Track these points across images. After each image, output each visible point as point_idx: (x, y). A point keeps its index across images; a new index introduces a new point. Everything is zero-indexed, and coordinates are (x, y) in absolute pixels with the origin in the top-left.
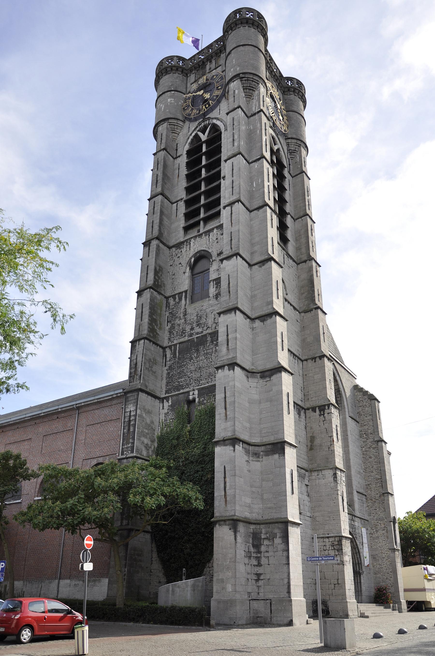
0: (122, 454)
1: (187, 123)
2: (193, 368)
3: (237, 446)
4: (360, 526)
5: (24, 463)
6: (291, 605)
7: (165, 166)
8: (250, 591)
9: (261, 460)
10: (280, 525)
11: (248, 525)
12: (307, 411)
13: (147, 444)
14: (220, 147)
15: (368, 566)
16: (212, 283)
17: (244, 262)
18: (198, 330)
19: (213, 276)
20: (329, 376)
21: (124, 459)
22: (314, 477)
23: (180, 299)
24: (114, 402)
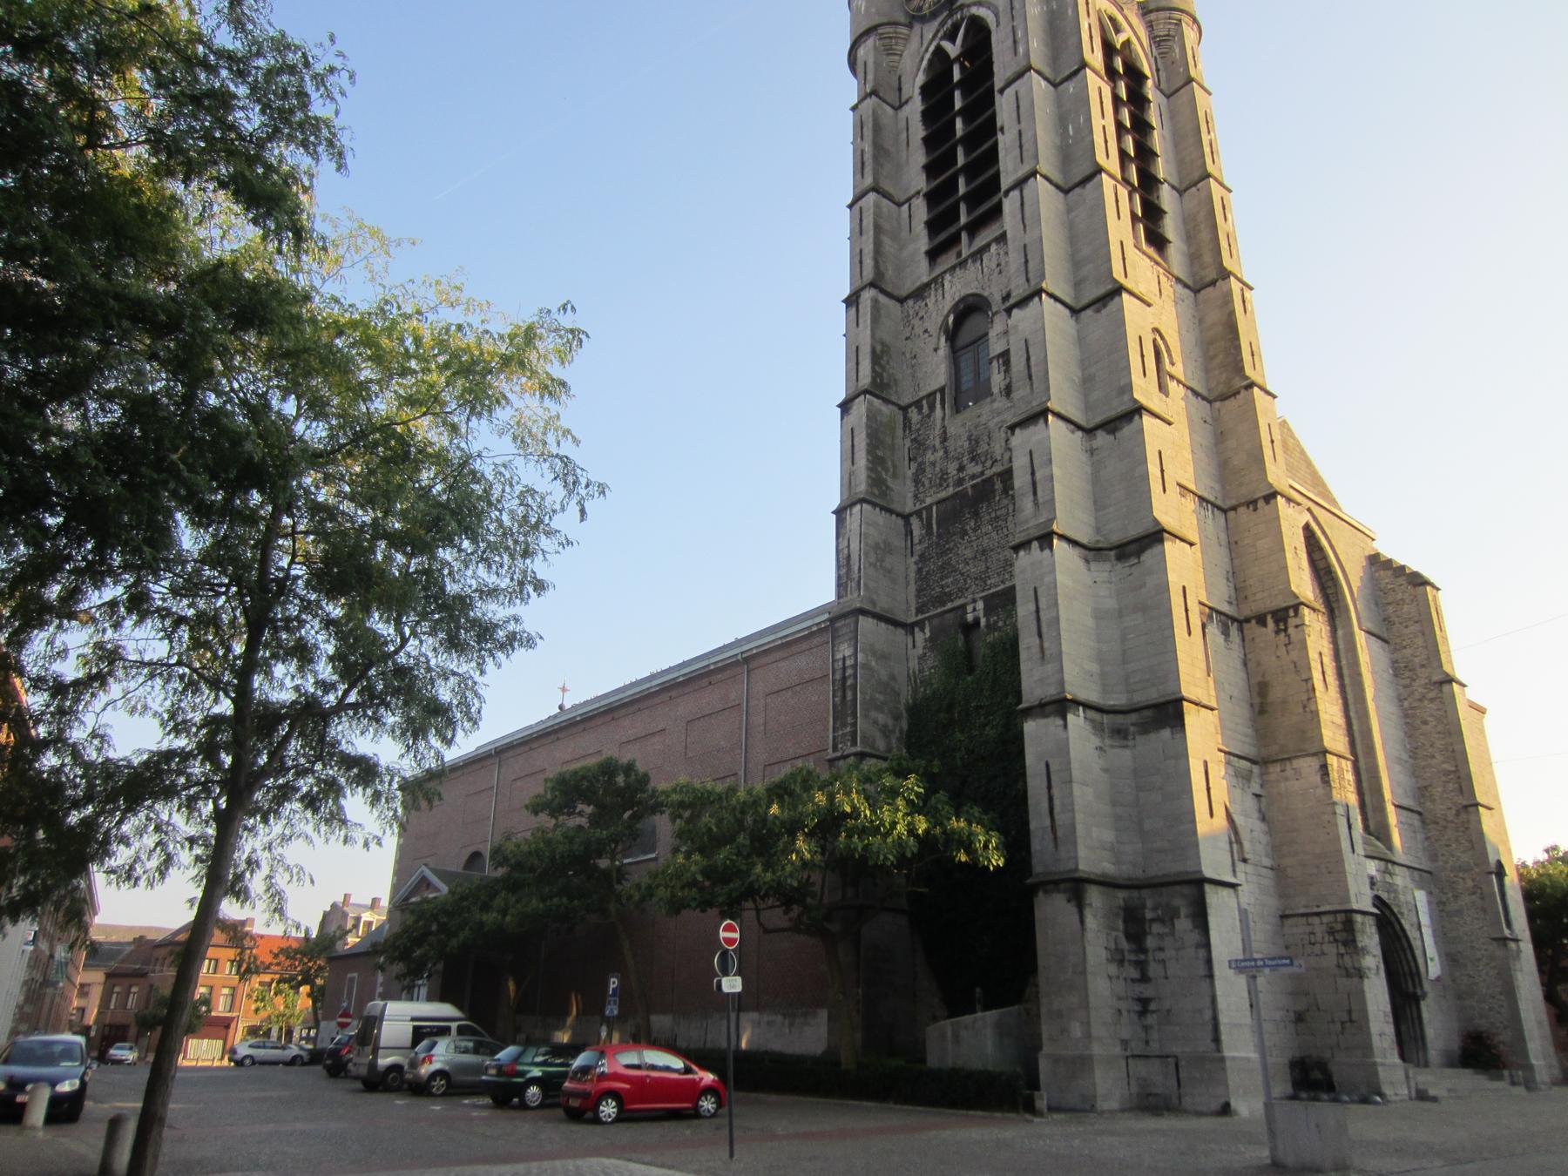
0: (835, 749)
1: (917, 27)
2: (968, 553)
3: (1070, 717)
4: (1410, 885)
5: (645, 779)
6: (1224, 1069)
7: (877, 129)
8: (1125, 1036)
9: (1131, 743)
10: (1186, 890)
11: (1110, 890)
12: (1246, 626)
13: (885, 726)
14: (990, 63)
15: (1438, 979)
16: (995, 363)
17: (1059, 305)
18: (973, 469)
19: (996, 347)
20: (1294, 543)
21: (838, 759)
22: (1272, 777)
23: (932, 408)
24: (816, 641)
